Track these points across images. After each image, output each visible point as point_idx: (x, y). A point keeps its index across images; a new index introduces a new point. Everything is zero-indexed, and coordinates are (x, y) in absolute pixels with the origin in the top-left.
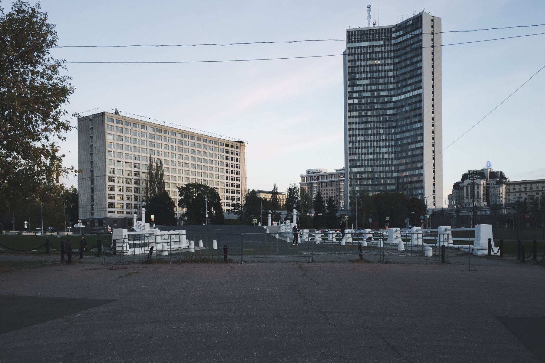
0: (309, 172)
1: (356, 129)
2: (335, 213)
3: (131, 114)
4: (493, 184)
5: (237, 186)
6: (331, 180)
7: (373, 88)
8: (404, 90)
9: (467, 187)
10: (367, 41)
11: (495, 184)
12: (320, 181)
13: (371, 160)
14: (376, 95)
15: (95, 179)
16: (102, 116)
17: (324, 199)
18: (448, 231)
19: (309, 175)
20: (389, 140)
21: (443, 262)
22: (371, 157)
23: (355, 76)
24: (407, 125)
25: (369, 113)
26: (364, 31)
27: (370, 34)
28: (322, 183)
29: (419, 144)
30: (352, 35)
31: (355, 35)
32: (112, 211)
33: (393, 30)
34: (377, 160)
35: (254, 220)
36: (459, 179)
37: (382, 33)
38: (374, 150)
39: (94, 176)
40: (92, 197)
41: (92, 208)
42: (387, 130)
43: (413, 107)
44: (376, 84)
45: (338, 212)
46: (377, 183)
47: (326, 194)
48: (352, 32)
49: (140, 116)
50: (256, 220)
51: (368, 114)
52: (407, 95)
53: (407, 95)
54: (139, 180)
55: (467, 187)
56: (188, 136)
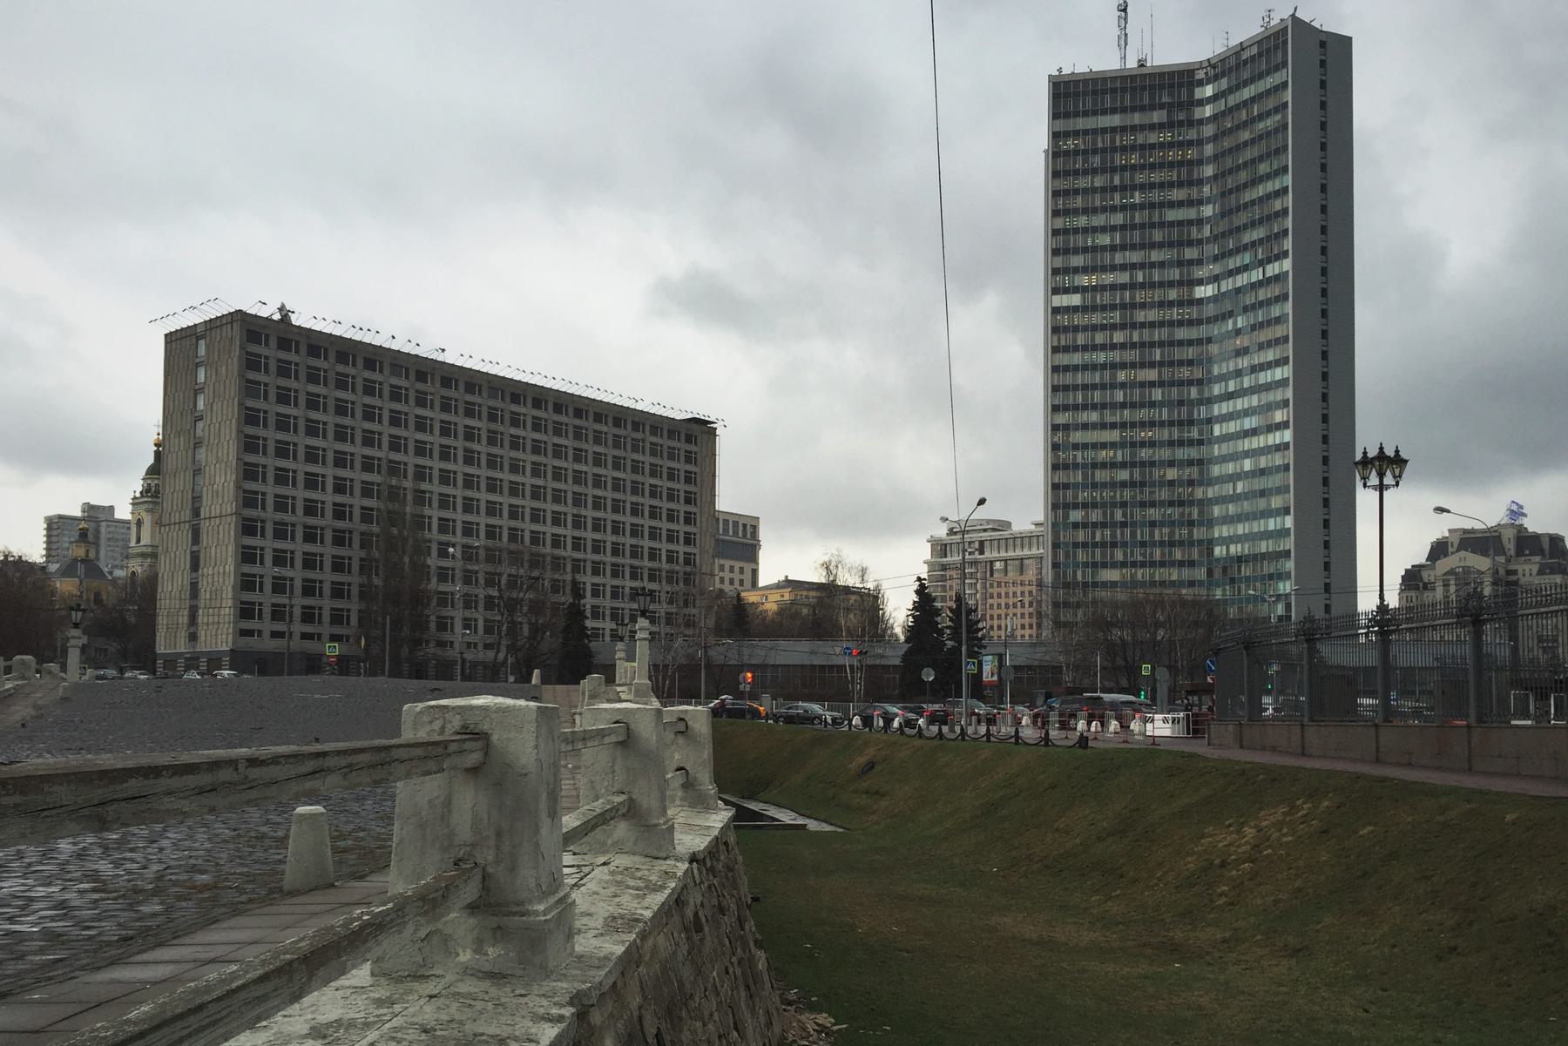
1: (1075, 388)
2: (976, 649)
3: (329, 320)
4: (1527, 572)
5: (687, 562)
6: (1019, 553)
7: (1135, 257)
8: (1233, 263)
9: (1444, 580)
10: (1114, 111)
11: (1535, 571)
12: (988, 555)
13: (1123, 484)
14: (1140, 279)
15: (204, 525)
16: (229, 326)
17: (938, 604)
19: (953, 537)
20: (1181, 423)
21: (1470, 770)
22: (1124, 475)
23: (1113, 258)
24: (1238, 373)
25: (1118, 337)
26: (1105, 79)
27: (1124, 90)
28: (992, 562)
29: (1278, 434)
30: (1067, 95)
31: (1077, 94)
32: (254, 631)
33: (1197, 77)
34: (1143, 484)
36: (1421, 557)
37: (1162, 87)
38: (1133, 455)
39: (202, 516)
42: (1175, 390)
43: (1261, 315)
44: (1142, 247)
45: (985, 647)
46: (1140, 558)
47: (1003, 595)
48: (1067, 83)
51: (1115, 341)
52: (1241, 280)
53: (1241, 280)
54: (350, 532)
55: (1444, 580)
56: (662, 429)
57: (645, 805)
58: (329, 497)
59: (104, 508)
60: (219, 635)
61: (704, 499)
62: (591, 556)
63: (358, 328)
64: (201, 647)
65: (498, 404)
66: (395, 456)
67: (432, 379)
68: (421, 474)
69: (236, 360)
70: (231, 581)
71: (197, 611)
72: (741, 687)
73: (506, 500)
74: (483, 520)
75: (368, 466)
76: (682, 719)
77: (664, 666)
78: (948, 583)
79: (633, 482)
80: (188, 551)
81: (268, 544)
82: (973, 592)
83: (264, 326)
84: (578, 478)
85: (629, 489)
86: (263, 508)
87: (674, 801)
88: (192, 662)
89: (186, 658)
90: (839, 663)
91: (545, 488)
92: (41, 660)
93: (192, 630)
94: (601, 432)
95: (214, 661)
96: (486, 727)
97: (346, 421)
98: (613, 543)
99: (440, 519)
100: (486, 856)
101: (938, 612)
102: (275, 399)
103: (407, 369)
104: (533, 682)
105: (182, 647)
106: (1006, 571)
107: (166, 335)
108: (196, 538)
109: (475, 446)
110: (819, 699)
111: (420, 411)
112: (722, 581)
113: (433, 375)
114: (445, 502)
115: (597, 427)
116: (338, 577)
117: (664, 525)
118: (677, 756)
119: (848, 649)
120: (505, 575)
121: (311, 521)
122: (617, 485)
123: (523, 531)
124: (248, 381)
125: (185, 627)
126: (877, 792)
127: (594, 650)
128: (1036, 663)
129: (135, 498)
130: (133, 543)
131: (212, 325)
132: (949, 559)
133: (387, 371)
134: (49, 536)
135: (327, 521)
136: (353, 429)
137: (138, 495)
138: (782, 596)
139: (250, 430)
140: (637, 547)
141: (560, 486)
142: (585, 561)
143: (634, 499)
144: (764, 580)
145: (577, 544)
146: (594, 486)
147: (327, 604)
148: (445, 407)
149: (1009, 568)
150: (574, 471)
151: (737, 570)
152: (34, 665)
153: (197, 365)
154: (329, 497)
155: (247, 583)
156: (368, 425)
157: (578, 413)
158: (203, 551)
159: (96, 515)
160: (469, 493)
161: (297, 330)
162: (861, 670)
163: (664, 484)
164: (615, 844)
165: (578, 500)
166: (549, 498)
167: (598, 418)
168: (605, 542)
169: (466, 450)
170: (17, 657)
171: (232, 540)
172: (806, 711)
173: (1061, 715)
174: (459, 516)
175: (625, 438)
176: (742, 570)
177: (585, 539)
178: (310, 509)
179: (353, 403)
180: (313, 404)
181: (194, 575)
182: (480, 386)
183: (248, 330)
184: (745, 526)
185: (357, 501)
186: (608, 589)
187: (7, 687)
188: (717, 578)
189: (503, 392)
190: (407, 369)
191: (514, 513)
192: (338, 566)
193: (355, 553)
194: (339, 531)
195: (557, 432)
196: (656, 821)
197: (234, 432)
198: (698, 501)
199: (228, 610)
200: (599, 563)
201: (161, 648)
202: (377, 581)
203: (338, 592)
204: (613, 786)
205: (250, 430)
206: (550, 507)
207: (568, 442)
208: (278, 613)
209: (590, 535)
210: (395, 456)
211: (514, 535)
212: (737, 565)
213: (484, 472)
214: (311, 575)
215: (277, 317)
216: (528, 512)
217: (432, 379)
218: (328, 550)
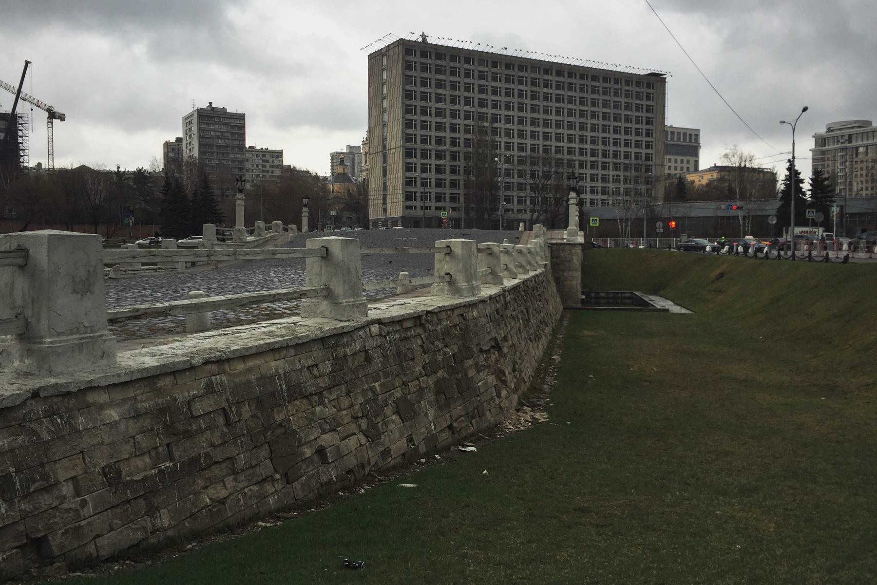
0: (832, 129)
2: (828, 203)
3: (446, 38)
12: (854, 144)
15: (388, 153)
18: (445, 246)
28: (857, 148)
35: (593, 220)
39: (387, 148)
40: (385, 184)
41: (385, 203)
49: (565, 57)
50: (596, 220)
57: (337, 291)
58: (448, 134)
59: (356, 147)
60: (396, 210)
62: (589, 158)
63: (460, 41)
64: (388, 216)
65: (537, 76)
66: (481, 110)
67: (500, 66)
68: (495, 119)
69: (400, 65)
70: (401, 181)
71: (386, 197)
72: (658, 230)
73: (541, 130)
74: (529, 142)
75: (467, 116)
76: (448, 247)
77: (626, 219)
78: (826, 163)
80: (382, 168)
81: (418, 161)
82: (843, 167)
83: (413, 46)
84: (582, 114)
85: (612, 118)
86: (416, 142)
87: (444, 292)
88: (385, 222)
89: (382, 221)
90: (733, 215)
91: (563, 121)
92: (286, 222)
93: (384, 207)
94: (595, 87)
95: (395, 222)
96: (27, 246)
97: (456, 93)
98: (602, 150)
99: (506, 143)
100: (28, 313)
101: (802, 181)
103: (487, 61)
104: (520, 229)
105: (380, 216)
106: (867, 153)
108: (385, 161)
109: (524, 101)
110: (704, 236)
111: (494, 84)
112: (670, 168)
113: (501, 63)
114: (508, 133)
115: (593, 83)
117: (633, 138)
118: (446, 267)
119: (730, 205)
120: (503, 170)
121: (439, 148)
122: (605, 117)
123: (551, 146)
124: (407, 76)
125: (381, 206)
126: (719, 291)
127: (585, 212)
128: (871, 211)
129: (364, 141)
130: (363, 165)
131: (389, 48)
132: (827, 147)
133: (476, 64)
134: (332, 166)
135: (447, 147)
136: (459, 97)
137: (365, 140)
138: (712, 176)
139: (408, 102)
140: (617, 151)
141: (572, 119)
142: (586, 161)
143: (615, 124)
144: (704, 165)
145: (582, 152)
146: (591, 118)
147: (448, 191)
148: (508, 81)
149: (869, 151)
151: (685, 161)
152: (281, 226)
153: (383, 70)
154: (448, 134)
155: (408, 182)
156: (467, 94)
157: (605, 80)
158: (388, 167)
159: (352, 151)
160: (521, 127)
161: (430, 46)
162: (749, 218)
163: (633, 114)
164: (321, 313)
165: (582, 127)
166: (566, 126)
167: (594, 78)
168: (598, 150)
169: (519, 103)
170: (274, 222)
171: (401, 160)
172: (697, 244)
173: (867, 243)
174: (516, 140)
175: (610, 89)
176: (688, 162)
177: (586, 149)
178: (439, 142)
179: (459, 83)
180: (439, 85)
181: (384, 178)
182: (526, 67)
183: (406, 49)
184: (690, 135)
185: (462, 136)
186: (600, 177)
187: (267, 236)
188: (666, 168)
189: (539, 69)
190: (487, 61)
191: (546, 137)
192: (453, 171)
193: (461, 163)
195: (570, 89)
196: (341, 301)
197: (400, 103)
198: (654, 122)
199: (400, 196)
200: (595, 162)
201: (371, 217)
202: (472, 178)
203: (454, 184)
204: (321, 282)
205: (408, 102)
206: (566, 132)
207: (576, 94)
208: (425, 197)
209: (589, 146)
210: (481, 110)
211: (546, 149)
212: (685, 159)
213: (529, 115)
214: (440, 176)
215: (420, 40)
216: (553, 135)
217: (500, 66)
218: (447, 163)
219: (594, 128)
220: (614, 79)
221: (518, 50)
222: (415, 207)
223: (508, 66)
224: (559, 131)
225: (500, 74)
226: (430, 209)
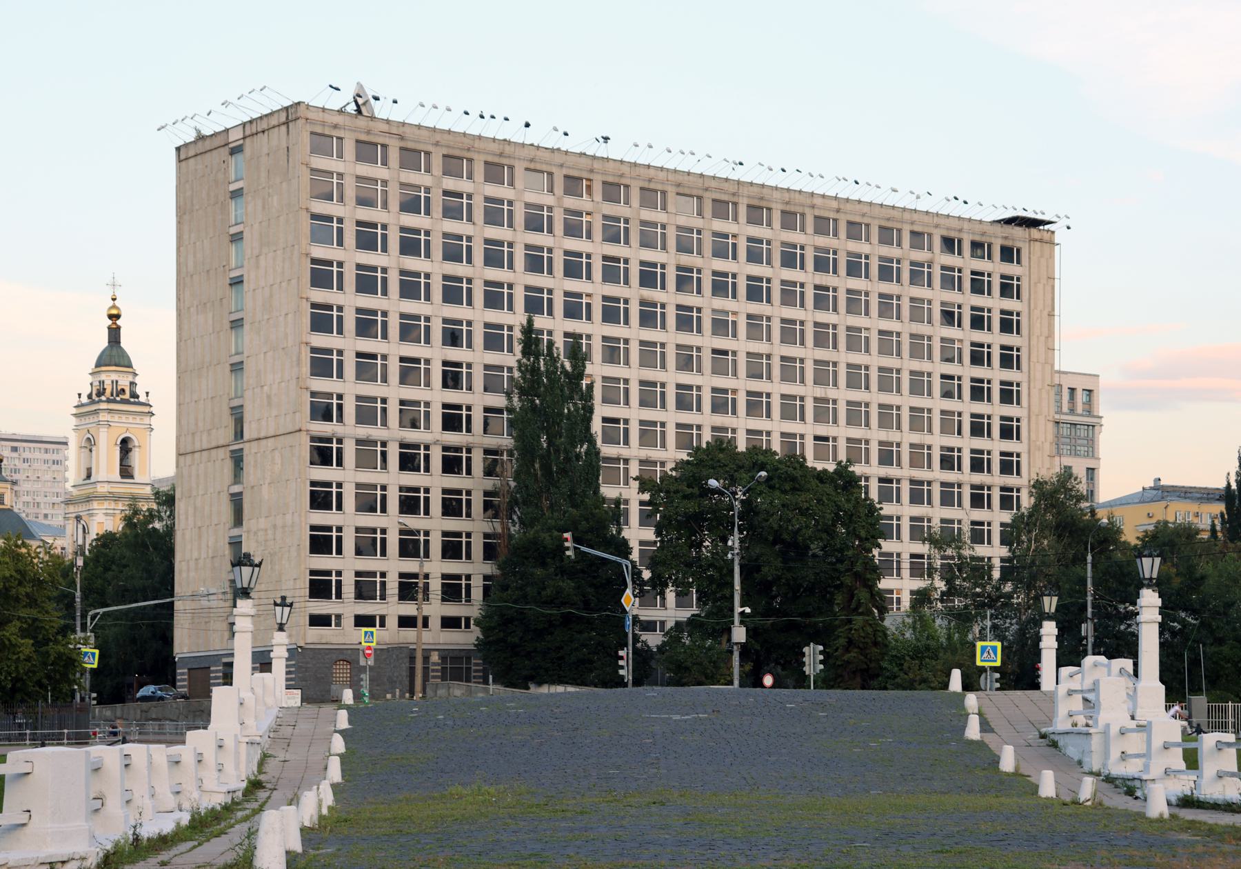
15: (250, 451)
49: (777, 169)
61: (1034, 359)
79: (912, 336)
96: (101, 855)
102: (354, 242)
107: (178, 149)
116: (453, 524)
135: (434, 435)
137: (85, 400)
146: (849, 348)
150: (816, 324)
166: (776, 372)
192: (452, 506)
193: (474, 483)
194: (321, 440)
208: (409, 588)
218: (435, 481)
219: (856, 377)
220: (913, 233)
221: (643, 145)
222: (383, 618)
223: (612, 191)
224: (756, 386)
225: (588, 214)
226: (382, 625)
